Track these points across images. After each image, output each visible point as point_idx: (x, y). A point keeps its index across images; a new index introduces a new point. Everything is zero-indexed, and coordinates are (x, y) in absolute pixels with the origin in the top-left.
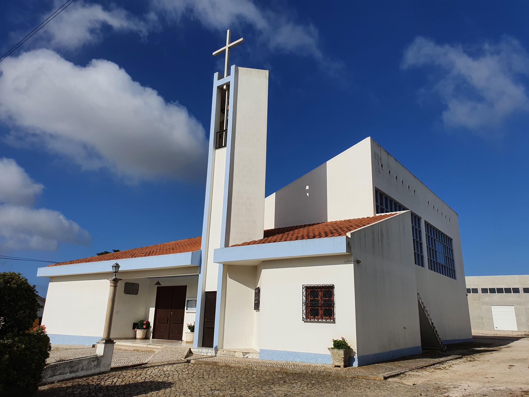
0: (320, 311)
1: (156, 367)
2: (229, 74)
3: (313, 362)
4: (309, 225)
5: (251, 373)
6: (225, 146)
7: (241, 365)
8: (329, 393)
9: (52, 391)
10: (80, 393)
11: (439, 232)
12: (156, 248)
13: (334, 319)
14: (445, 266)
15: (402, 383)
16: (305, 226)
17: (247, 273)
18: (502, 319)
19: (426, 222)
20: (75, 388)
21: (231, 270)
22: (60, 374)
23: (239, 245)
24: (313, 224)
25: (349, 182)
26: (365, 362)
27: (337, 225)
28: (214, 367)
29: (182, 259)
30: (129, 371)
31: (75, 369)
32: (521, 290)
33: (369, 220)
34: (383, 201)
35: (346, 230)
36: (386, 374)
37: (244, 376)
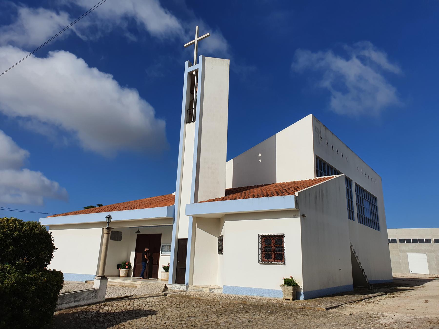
0: (273, 256)
1: (140, 299)
2: (197, 62)
3: (267, 296)
4: (262, 186)
5: (217, 304)
6: (194, 121)
7: (209, 298)
8: (283, 320)
9: (62, 316)
10: (84, 318)
11: (367, 192)
12: (136, 203)
13: (284, 262)
14: (371, 220)
15: (341, 313)
16: (258, 186)
17: (213, 224)
18: (416, 264)
19: (356, 184)
20: (80, 313)
21: (199, 221)
22: (66, 303)
23: (206, 202)
24: (265, 185)
25: (294, 151)
26: (309, 296)
27: (285, 186)
28: (187, 300)
29: (159, 212)
30: (119, 302)
31: (78, 299)
32: (432, 241)
33: (311, 182)
34: (322, 167)
35: (294, 190)
36: (328, 306)
37: (212, 306)
